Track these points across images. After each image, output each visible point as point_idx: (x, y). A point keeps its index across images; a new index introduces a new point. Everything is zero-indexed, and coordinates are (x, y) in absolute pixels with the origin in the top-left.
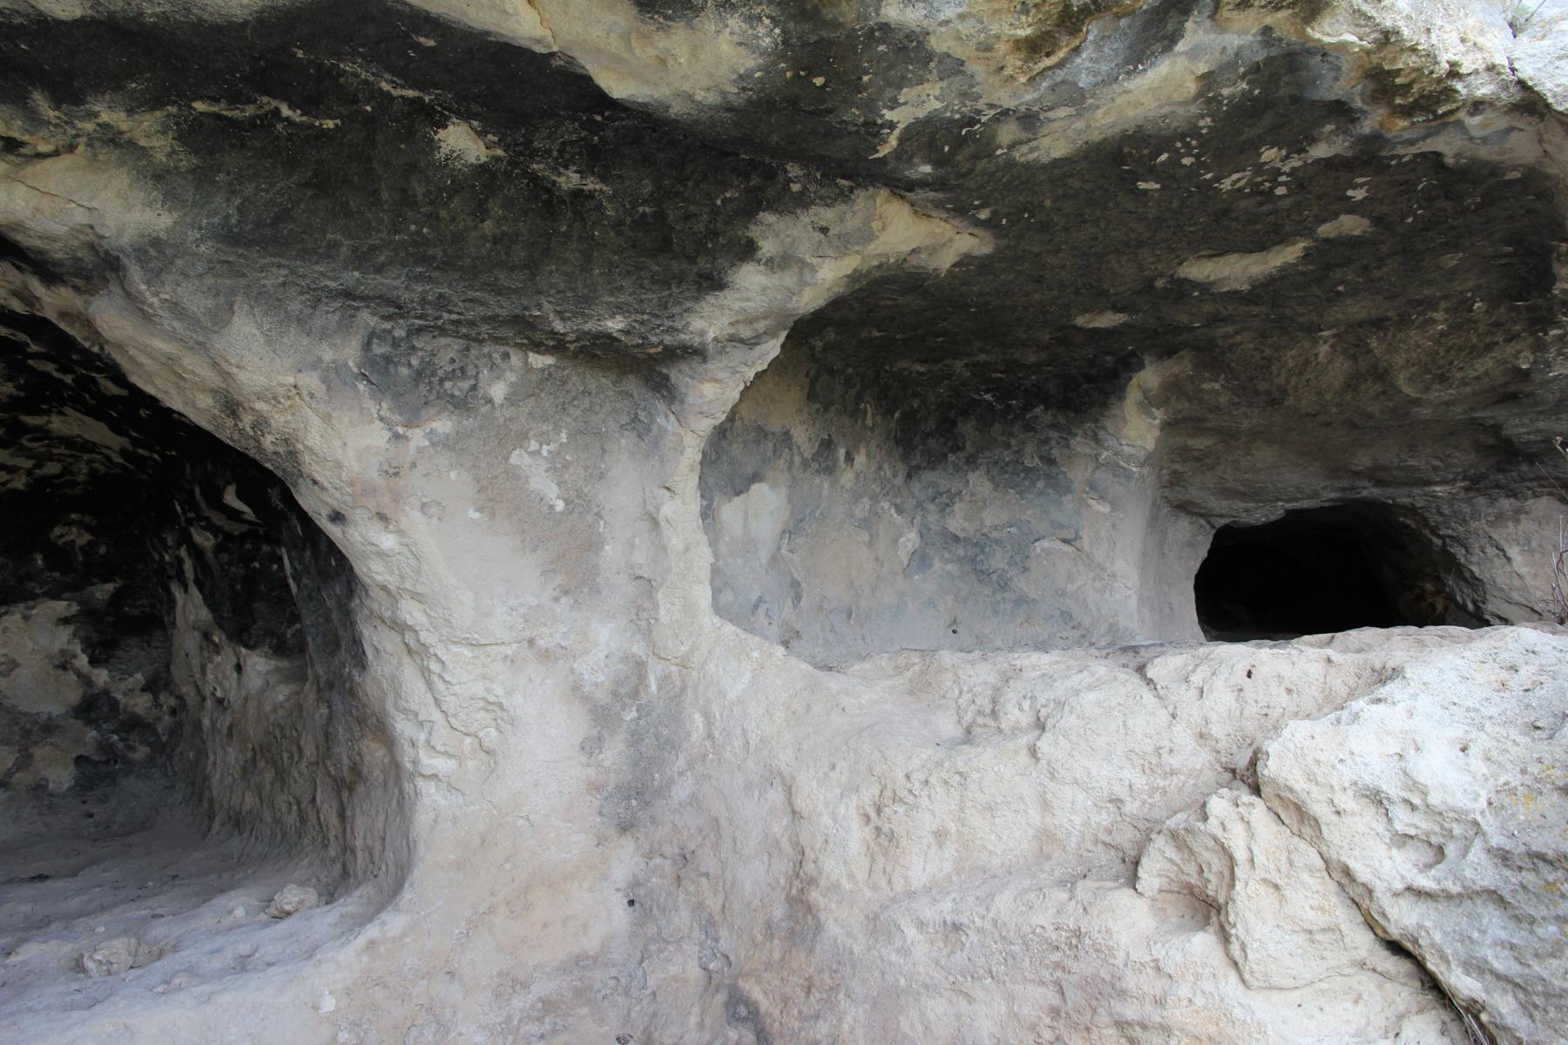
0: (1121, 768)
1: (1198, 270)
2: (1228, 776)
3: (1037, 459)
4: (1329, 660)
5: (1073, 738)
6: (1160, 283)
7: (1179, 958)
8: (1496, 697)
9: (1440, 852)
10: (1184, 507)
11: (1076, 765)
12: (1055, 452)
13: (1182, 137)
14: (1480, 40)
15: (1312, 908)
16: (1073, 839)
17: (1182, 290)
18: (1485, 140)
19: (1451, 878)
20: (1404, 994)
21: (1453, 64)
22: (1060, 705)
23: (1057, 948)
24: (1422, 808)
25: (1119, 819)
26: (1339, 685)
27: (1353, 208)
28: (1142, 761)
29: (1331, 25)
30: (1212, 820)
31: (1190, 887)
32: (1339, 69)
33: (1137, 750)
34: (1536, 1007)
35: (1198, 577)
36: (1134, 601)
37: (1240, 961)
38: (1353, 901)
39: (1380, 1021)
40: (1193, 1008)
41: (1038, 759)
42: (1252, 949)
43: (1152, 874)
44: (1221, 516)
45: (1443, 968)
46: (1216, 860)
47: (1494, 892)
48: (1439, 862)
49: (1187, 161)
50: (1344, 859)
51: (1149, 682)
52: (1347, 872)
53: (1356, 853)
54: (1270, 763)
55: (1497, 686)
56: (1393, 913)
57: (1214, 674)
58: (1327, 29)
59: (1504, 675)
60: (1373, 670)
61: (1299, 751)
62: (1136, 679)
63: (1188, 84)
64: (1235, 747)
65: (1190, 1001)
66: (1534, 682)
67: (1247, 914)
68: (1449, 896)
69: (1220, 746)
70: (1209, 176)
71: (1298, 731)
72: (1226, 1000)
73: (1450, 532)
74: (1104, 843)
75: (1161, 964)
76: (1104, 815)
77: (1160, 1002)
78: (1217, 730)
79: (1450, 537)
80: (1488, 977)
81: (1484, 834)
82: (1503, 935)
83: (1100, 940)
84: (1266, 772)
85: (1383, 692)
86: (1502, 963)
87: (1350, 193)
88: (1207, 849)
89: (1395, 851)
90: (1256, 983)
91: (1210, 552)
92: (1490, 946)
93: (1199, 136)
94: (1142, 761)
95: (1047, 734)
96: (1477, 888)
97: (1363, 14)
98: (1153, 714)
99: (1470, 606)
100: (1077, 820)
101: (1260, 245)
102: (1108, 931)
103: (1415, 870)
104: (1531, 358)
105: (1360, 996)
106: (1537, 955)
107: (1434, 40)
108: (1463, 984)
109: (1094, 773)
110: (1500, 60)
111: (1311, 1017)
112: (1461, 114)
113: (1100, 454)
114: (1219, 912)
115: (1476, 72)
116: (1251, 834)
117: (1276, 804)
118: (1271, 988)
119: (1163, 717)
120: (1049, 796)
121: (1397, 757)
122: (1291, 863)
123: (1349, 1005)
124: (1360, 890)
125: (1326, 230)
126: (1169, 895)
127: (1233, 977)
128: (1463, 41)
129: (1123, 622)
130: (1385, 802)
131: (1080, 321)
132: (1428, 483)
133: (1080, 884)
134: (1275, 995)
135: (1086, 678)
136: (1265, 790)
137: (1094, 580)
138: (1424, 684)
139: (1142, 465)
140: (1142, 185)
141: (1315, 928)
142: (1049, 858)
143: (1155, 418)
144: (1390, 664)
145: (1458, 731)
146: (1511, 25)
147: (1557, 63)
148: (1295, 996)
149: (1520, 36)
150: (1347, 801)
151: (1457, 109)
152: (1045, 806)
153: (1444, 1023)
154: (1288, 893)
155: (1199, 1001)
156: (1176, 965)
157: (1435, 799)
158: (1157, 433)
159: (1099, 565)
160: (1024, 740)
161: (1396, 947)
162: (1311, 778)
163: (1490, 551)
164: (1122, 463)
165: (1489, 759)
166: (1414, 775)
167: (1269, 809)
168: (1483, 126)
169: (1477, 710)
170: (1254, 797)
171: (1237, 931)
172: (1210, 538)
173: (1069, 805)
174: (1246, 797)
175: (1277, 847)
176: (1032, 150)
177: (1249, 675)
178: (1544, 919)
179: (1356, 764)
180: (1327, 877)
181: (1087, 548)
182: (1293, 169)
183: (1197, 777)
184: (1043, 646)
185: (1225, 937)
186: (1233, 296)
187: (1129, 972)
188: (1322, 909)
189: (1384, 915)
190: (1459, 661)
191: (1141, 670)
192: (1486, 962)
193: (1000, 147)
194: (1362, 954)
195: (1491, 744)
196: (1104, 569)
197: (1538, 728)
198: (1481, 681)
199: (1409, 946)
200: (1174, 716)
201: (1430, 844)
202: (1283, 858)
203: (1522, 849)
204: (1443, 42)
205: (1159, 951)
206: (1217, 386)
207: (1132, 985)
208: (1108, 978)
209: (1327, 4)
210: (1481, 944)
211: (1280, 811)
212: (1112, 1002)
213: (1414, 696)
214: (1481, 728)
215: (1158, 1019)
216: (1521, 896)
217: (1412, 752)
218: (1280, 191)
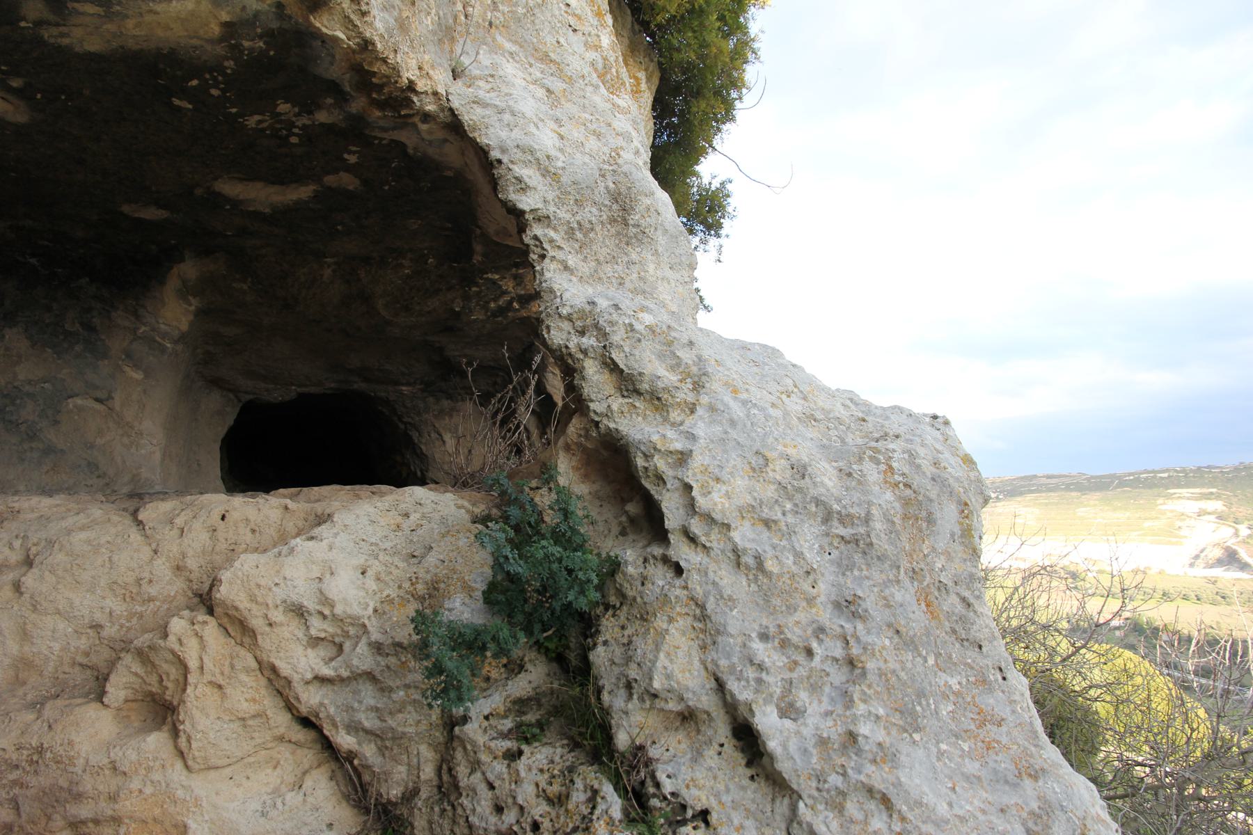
0: (104, 598)
1: (231, 188)
2: (196, 600)
3: (78, 325)
4: (286, 508)
5: (60, 573)
6: (199, 192)
7: (134, 757)
8: (392, 535)
9: (340, 648)
10: (216, 383)
11: (59, 597)
12: (96, 321)
13: (211, 71)
14: (431, 72)
15: (247, 700)
16: (52, 664)
17: (216, 201)
18: (431, 143)
19: (344, 666)
20: (308, 756)
21: (411, 82)
22: (51, 543)
23: (17, 767)
24: (330, 618)
25: (97, 642)
26: (290, 527)
27: (349, 169)
28: (124, 591)
29: (328, 20)
30: (172, 638)
31: (151, 694)
32: (333, 56)
33: (119, 582)
34: (386, 748)
35: (223, 441)
36: (158, 456)
37: (185, 751)
38: (279, 692)
39: (290, 779)
40: (142, 797)
41: (21, 594)
42: (196, 740)
43: (117, 691)
44: (246, 393)
45: (334, 732)
46: (174, 671)
47: (370, 673)
48: (339, 656)
49: (215, 92)
50: (272, 660)
51: (140, 523)
52: (274, 669)
53: (281, 654)
54: (222, 588)
55: (393, 527)
56: (304, 696)
57: (194, 517)
58: (326, 22)
59: (399, 519)
60: (317, 516)
61: (245, 578)
62: (128, 521)
63: (212, 26)
64: (205, 576)
65: (140, 791)
66: (417, 525)
67: (194, 711)
68: (342, 680)
69: (192, 576)
70: (234, 110)
71: (247, 562)
72: (172, 785)
73: (410, 420)
74: (81, 665)
75: (118, 765)
76: (84, 640)
77: (113, 798)
78: (192, 563)
79: (410, 423)
80: (361, 733)
81: (368, 633)
82: (372, 702)
83: (62, 752)
84: (218, 596)
85: (316, 531)
86: (369, 722)
87: (346, 156)
88: (166, 661)
89: (309, 650)
90: (197, 767)
91: (236, 421)
92: (364, 712)
93: (225, 74)
94: (124, 591)
95: (35, 570)
96: (360, 671)
97: (351, 21)
98: (137, 551)
99: (419, 473)
100: (57, 646)
101: (280, 179)
102: (71, 743)
103: (322, 663)
104: (461, 304)
105: (278, 763)
106: (391, 713)
107: (399, 60)
108: (345, 741)
109: (77, 602)
110: (442, 91)
111: (239, 786)
112: (416, 119)
113: (139, 329)
114: (174, 712)
115: (426, 93)
116: (203, 647)
117: (225, 621)
118: (209, 768)
119: (146, 552)
120: (29, 627)
121: (317, 580)
122: (232, 667)
123: (269, 771)
124: (282, 682)
125: (330, 180)
126: (134, 704)
127: (179, 765)
128: (420, 68)
129: (144, 473)
130: (306, 614)
131: (126, 209)
132: (397, 383)
133: (48, 705)
134: (213, 774)
135: (82, 519)
136: (218, 610)
137: (122, 435)
138: (345, 526)
139: (176, 342)
140: (177, 102)
141: (247, 715)
142: (24, 683)
143: (190, 305)
144: (328, 511)
145: (361, 560)
146: (453, 71)
147: (472, 105)
148: (228, 771)
149: (458, 80)
150: (277, 616)
151: (413, 115)
152: (25, 635)
153: (333, 771)
154: (228, 691)
155: (148, 790)
156: (131, 763)
157: (339, 610)
158: (191, 317)
159: (128, 423)
160: (10, 576)
161: (306, 722)
162: (253, 599)
163: (433, 435)
164: (157, 338)
165: (379, 579)
166: (326, 592)
167: (220, 625)
168: (430, 132)
169: (377, 545)
170: (208, 616)
171: (185, 727)
172: (237, 410)
173: (50, 633)
174: (202, 617)
175: (223, 655)
176: (62, 35)
177: (223, 518)
178: (398, 687)
179: (287, 586)
180: (260, 675)
181: (117, 408)
182: (304, 125)
183: (172, 601)
184: (47, 492)
185: (175, 733)
186: (257, 215)
187: (87, 777)
188: (254, 700)
189: (298, 699)
190: (372, 510)
191: (135, 514)
192: (361, 723)
193: (24, 19)
194: (282, 730)
195: (381, 568)
196: (132, 427)
197: (414, 556)
198: (383, 524)
199: (313, 719)
200: (156, 552)
201: (334, 642)
202: (227, 663)
203: (390, 641)
204: (406, 63)
205: (116, 754)
206: (245, 287)
207: (89, 787)
208: (65, 785)
209: (326, 4)
210: (358, 711)
211: (228, 626)
212: (68, 806)
213: (336, 535)
214: (376, 558)
215: (110, 812)
216: (386, 674)
217: (328, 576)
218: (294, 140)
